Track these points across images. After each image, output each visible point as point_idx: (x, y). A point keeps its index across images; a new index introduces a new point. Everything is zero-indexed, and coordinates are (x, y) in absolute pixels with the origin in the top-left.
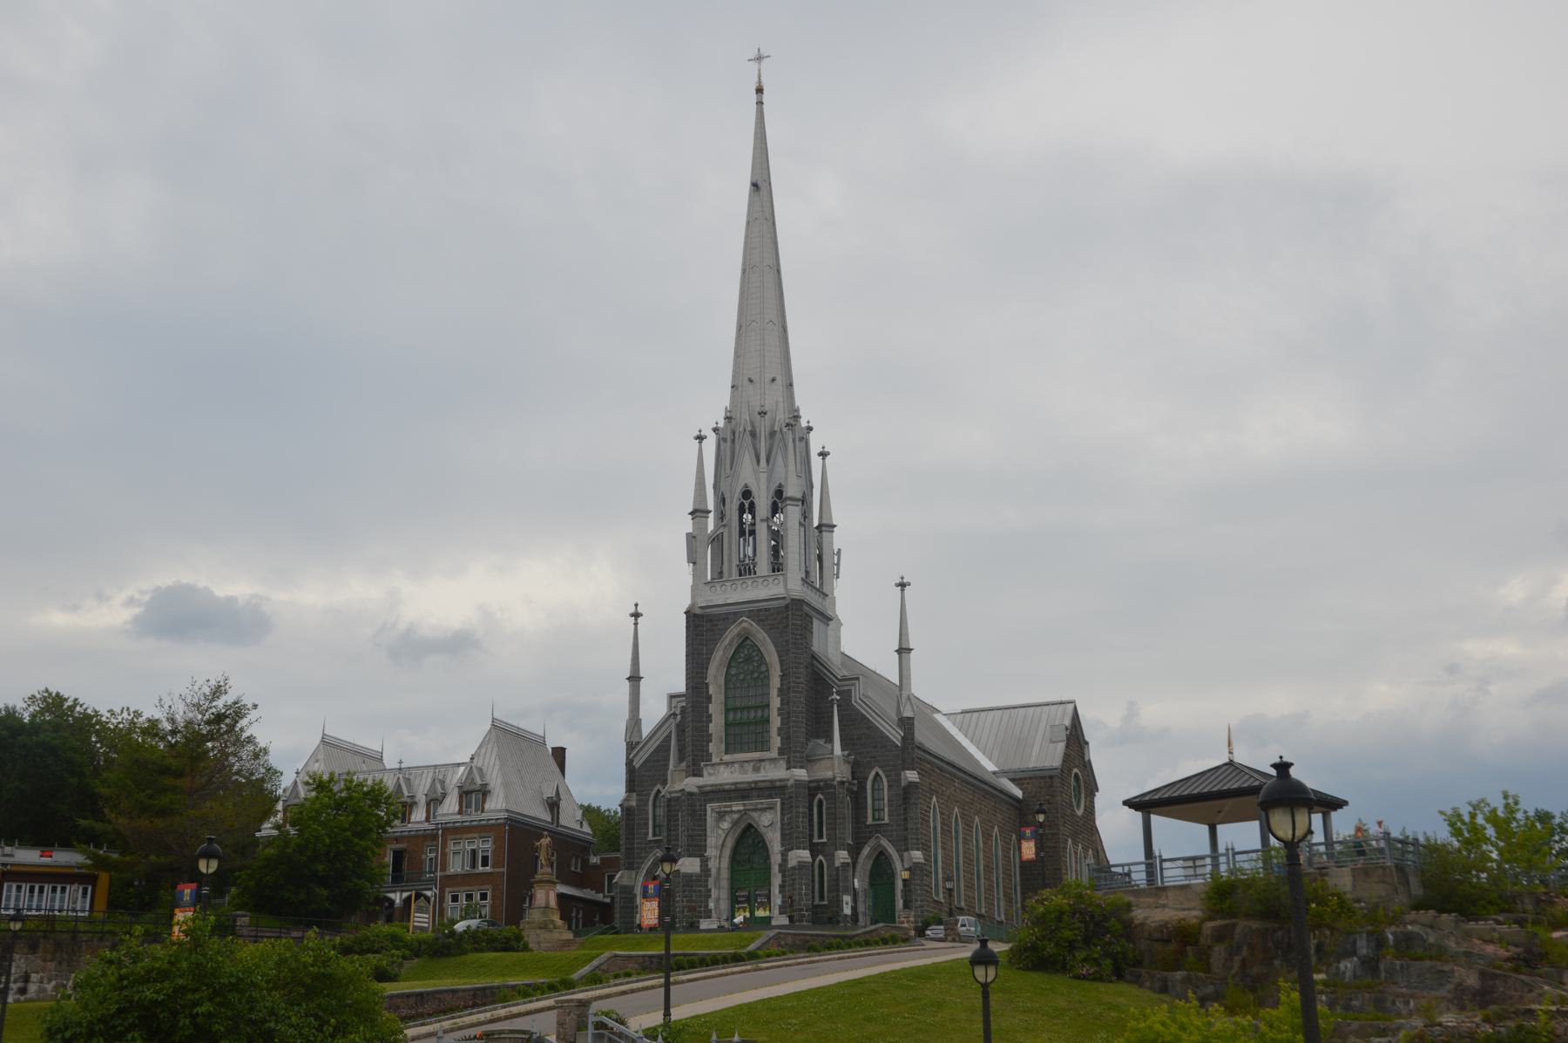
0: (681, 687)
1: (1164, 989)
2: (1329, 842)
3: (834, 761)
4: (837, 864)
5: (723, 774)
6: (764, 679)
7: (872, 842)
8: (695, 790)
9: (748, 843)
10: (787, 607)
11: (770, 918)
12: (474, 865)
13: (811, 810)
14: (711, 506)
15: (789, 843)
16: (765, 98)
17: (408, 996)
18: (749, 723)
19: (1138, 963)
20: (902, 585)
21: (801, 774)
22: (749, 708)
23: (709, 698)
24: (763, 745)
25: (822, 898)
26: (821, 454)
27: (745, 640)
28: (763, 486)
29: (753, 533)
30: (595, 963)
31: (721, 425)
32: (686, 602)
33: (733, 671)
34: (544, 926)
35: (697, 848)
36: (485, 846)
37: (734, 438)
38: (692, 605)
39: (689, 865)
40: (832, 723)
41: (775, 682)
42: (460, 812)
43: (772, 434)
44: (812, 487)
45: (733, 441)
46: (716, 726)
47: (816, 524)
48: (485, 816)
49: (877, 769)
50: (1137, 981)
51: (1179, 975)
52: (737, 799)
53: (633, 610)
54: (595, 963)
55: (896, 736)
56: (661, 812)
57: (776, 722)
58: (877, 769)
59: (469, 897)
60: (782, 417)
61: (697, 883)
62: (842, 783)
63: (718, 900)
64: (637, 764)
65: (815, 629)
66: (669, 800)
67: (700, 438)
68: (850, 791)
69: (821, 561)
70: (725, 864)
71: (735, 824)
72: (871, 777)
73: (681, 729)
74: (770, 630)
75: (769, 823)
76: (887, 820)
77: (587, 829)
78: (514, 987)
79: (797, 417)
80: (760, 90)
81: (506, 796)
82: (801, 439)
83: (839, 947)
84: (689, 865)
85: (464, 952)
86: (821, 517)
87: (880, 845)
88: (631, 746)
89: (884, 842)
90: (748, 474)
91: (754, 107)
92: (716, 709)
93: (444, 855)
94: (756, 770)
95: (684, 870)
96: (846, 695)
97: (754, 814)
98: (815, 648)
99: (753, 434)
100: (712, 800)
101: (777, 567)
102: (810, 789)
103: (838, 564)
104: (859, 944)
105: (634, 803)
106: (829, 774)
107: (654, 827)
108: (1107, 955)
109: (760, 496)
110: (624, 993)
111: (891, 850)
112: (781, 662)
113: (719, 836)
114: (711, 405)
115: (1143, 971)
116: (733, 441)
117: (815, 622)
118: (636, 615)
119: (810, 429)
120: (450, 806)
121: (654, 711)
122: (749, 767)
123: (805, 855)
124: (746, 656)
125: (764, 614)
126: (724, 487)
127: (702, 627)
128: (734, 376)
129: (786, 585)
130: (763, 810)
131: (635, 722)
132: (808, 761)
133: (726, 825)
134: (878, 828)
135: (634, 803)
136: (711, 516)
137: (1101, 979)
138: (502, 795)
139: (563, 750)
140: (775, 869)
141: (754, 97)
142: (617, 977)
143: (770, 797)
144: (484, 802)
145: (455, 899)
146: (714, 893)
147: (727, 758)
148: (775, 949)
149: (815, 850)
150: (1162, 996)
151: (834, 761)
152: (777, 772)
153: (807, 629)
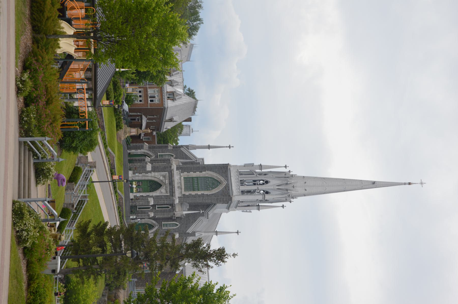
0: (206, 162)
1: (103, 296)
3: (181, 211)
4: (149, 213)
5: (178, 177)
6: (207, 189)
7: (156, 224)
8: (172, 168)
9: (155, 185)
10: (230, 196)
11: (132, 192)
12: (150, 97)
13: (166, 205)
14: (263, 171)
15: (155, 198)
17: (102, 112)
18: (193, 184)
19: (110, 290)
20: (238, 233)
21: (177, 201)
22: (198, 185)
23: (201, 172)
24: (186, 189)
25: (139, 208)
26: (283, 205)
28: (269, 188)
29: (255, 184)
30: (112, 153)
31: (291, 173)
32: (232, 163)
33: (210, 179)
34: (125, 132)
35: (154, 169)
36: (156, 101)
38: (230, 166)
39: (149, 167)
41: (206, 193)
42: (167, 92)
43: (287, 190)
44: (271, 203)
45: (285, 177)
46: (192, 174)
47: (260, 204)
48: (166, 100)
49: (179, 225)
50: (105, 289)
51: (106, 299)
52: (169, 182)
53: (231, 146)
54: (112, 153)
55: (190, 231)
56: (167, 157)
57: (193, 193)
58: (179, 225)
59: (140, 96)
60: (293, 193)
61: (143, 170)
62: (174, 214)
63: (138, 176)
64: (182, 149)
65: (224, 205)
66: (169, 160)
67: (286, 167)
68: (172, 217)
69: (248, 206)
70: (150, 178)
71: (162, 181)
73: (192, 163)
74: (222, 191)
75: (162, 192)
77: (164, 130)
78: (105, 135)
79: (293, 198)
80: (410, 184)
81: (172, 107)
82: (286, 199)
83: (120, 215)
84: (149, 167)
85: (115, 116)
86: (262, 206)
88: (187, 147)
89: (156, 228)
90: (273, 183)
91: (403, 182)
92: (198, 174)
93: (154, 88)
94: (178, 187)
95: (147, 165)
96: (203, 215)
97: (165, 187)
98: (218, 205)
99: (287, 184)
100: (169, 174)
101: (243, 192)
102: (173, 204)
103: (247, 212)
104: (121, 221)
105: (169, 148)
106: (177, 210)
107: (162, 155)
108: (112, 282)
110: (104, 162)
112: (212, 194)
113: (158, 176)
114: (298, 170)
115: (108, 291)
116: (285, 177)
117: (227, 205)
118: (230, 147)
119: (291, 202)
120: (168, 88)
121: (198, 154)
122: (179, 185)
123: (152, 203)
125: (228, 188)
126: (270, 175)
127: (224, 169)
128: (308, 177)
129: (237, 195)
130: (166, 190)
131: (195, 147)
132: (181, 203)
133: (161, 178)
135: (169, 148)
136: (260, 171)
137: (105, 281)
138: (172, 105)
139: (191, 121)
140: (148, 194)
142: (109, 158)
143: (170, 192)
144: (170, 100)
145: (140, 92)
146: (140, 175)
147: (182, 178)
148: (118, 197)
149: (154, 206)
150: (101, 295)
151: (181, 211)
152: (177, 194)
153: (224, 202)
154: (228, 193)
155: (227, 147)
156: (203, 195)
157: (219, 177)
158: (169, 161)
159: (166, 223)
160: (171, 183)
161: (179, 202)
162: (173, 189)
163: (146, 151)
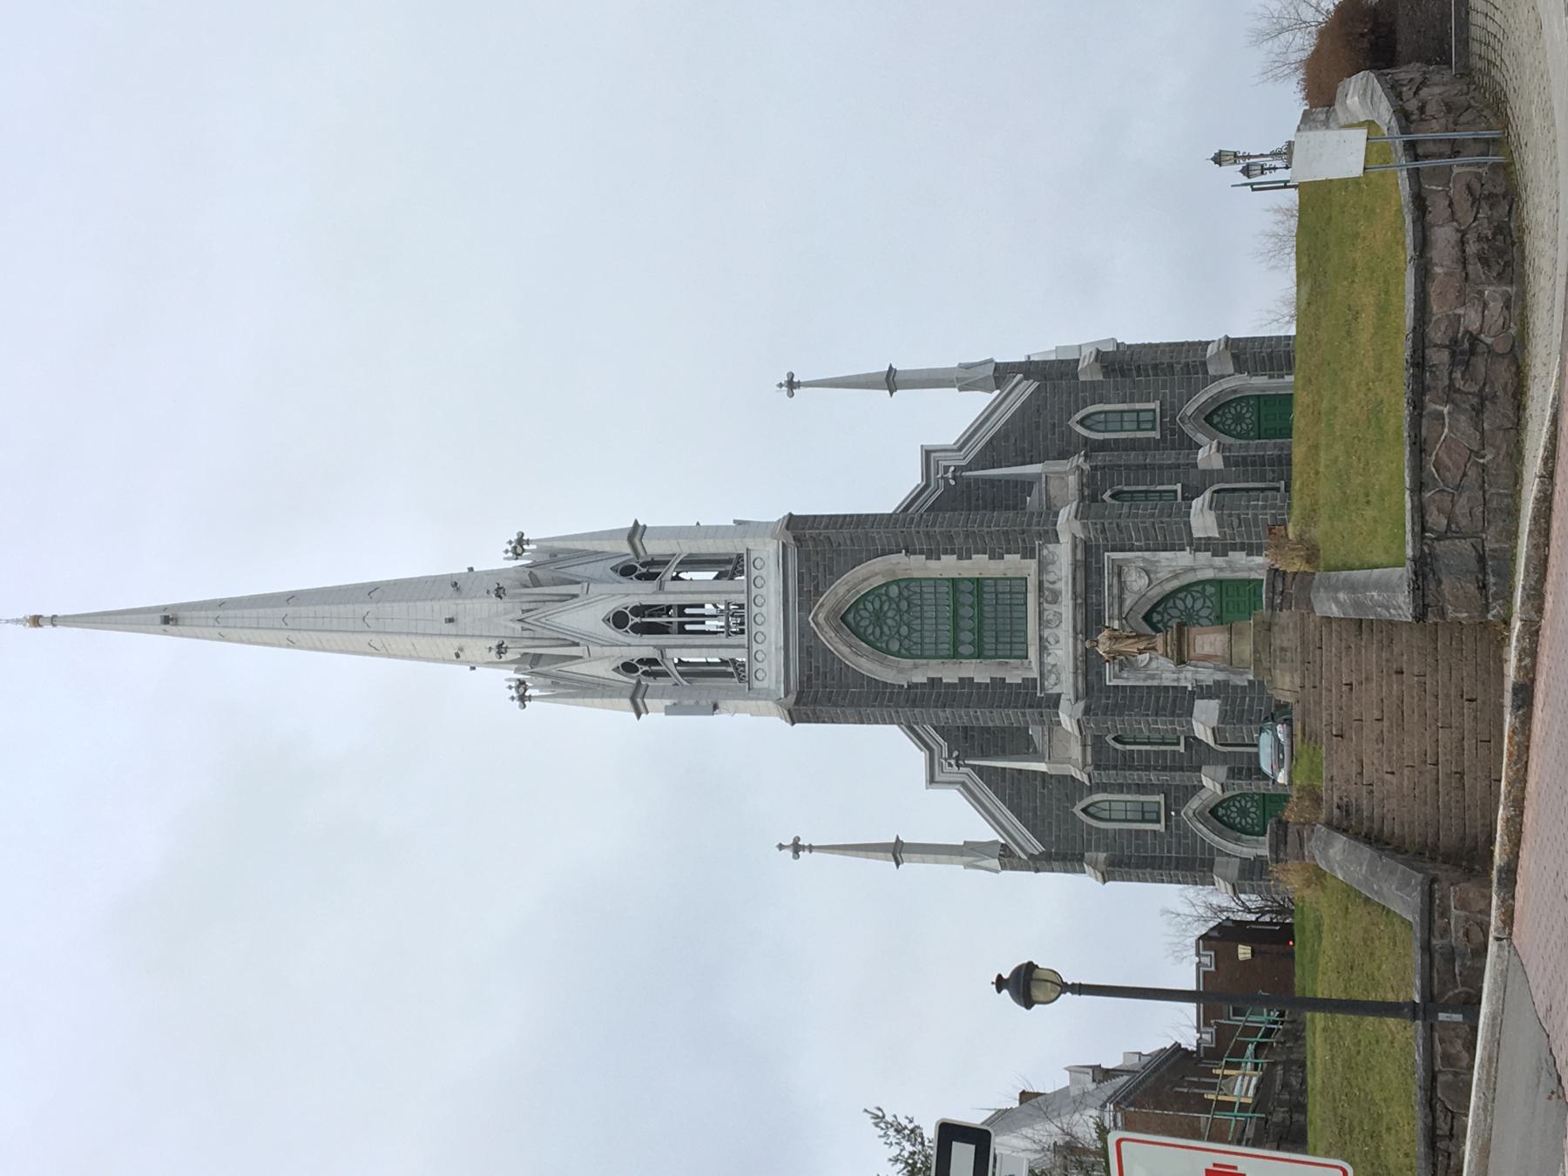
2: (1274, 731)
5: (1060, 654)
8: (1081, 705)
15: (1181, 539)
16: (48, 613)
20: (792, 385)
21: (1067, 718)
23: (933, 682)
27: (847, 620)
32: (776, 724)
37: (544, 669)
38: (778, 701)
40: (992, 482)
46: (980, 672)
53: (789, 853)
58: (1077, 810)
64: (1037, 847)
66: (1097, 767)
72: (1118, 746)
74: (833, 574)
76: (1155, 405)
80: (36, 621)
87: (1194, 417)
89: (1190, 408)
91: (60, 630)
94: (1056, 596)
100: (1101, 675)
105: (1102, 856)
106: (1072, 480)
107: (1143, 820)
109: (630, 619)
111: (1203, 397)
118: (797, 848)
121: (957, 816)
124: (870, 620)
127: (819, 694)
130: (1122, 587)
131: (969, 852)
134: (1169, 414)
135: (1102, 856)
139: (1023, 1094)
141: (47, 630)
143: (1100, 571)
149: (1191, 493)
151: (1062, 478)
152: (1062, 555)
154: (804, 558)
155: (811, 848)
156: (932, 554)
157: (846, 650)
158: (1100, 755)
159: (1139, 435)
160: (1090, 621)
161: (1057, 514)
162: (1080, 588)
163: (1230, 847)
